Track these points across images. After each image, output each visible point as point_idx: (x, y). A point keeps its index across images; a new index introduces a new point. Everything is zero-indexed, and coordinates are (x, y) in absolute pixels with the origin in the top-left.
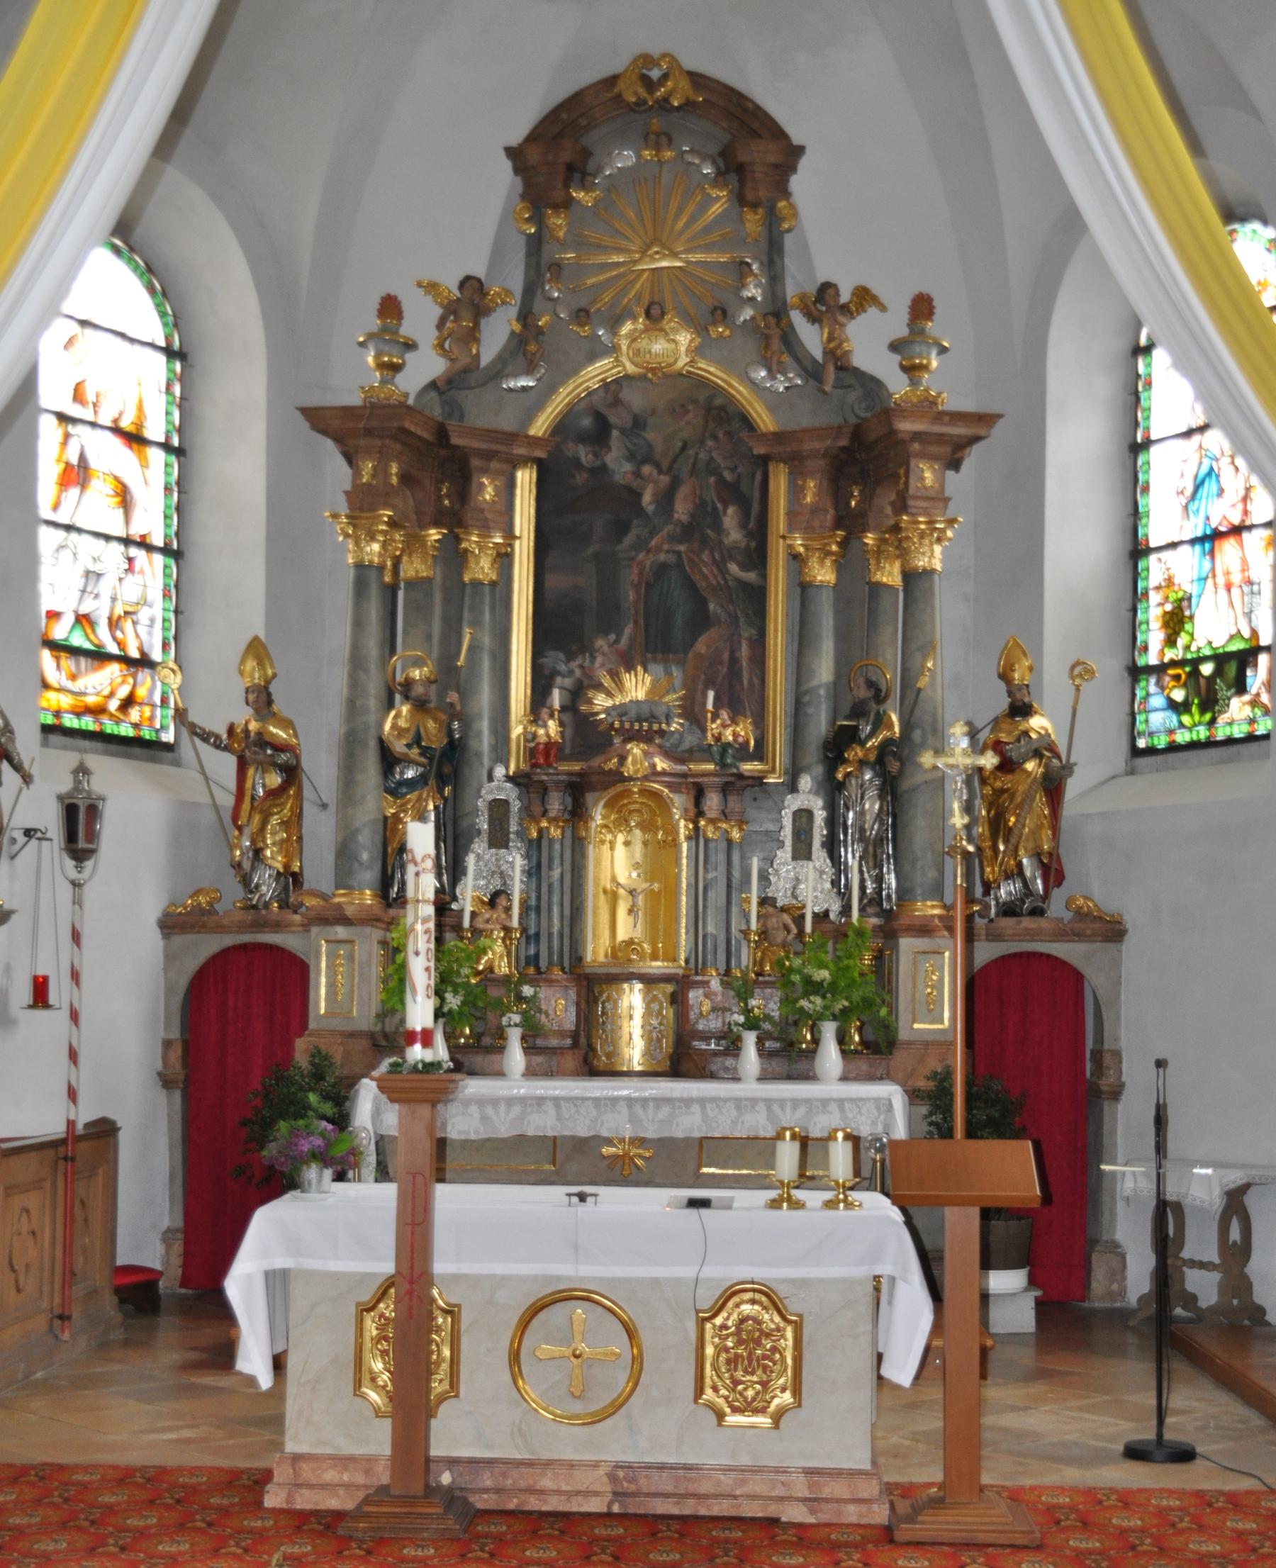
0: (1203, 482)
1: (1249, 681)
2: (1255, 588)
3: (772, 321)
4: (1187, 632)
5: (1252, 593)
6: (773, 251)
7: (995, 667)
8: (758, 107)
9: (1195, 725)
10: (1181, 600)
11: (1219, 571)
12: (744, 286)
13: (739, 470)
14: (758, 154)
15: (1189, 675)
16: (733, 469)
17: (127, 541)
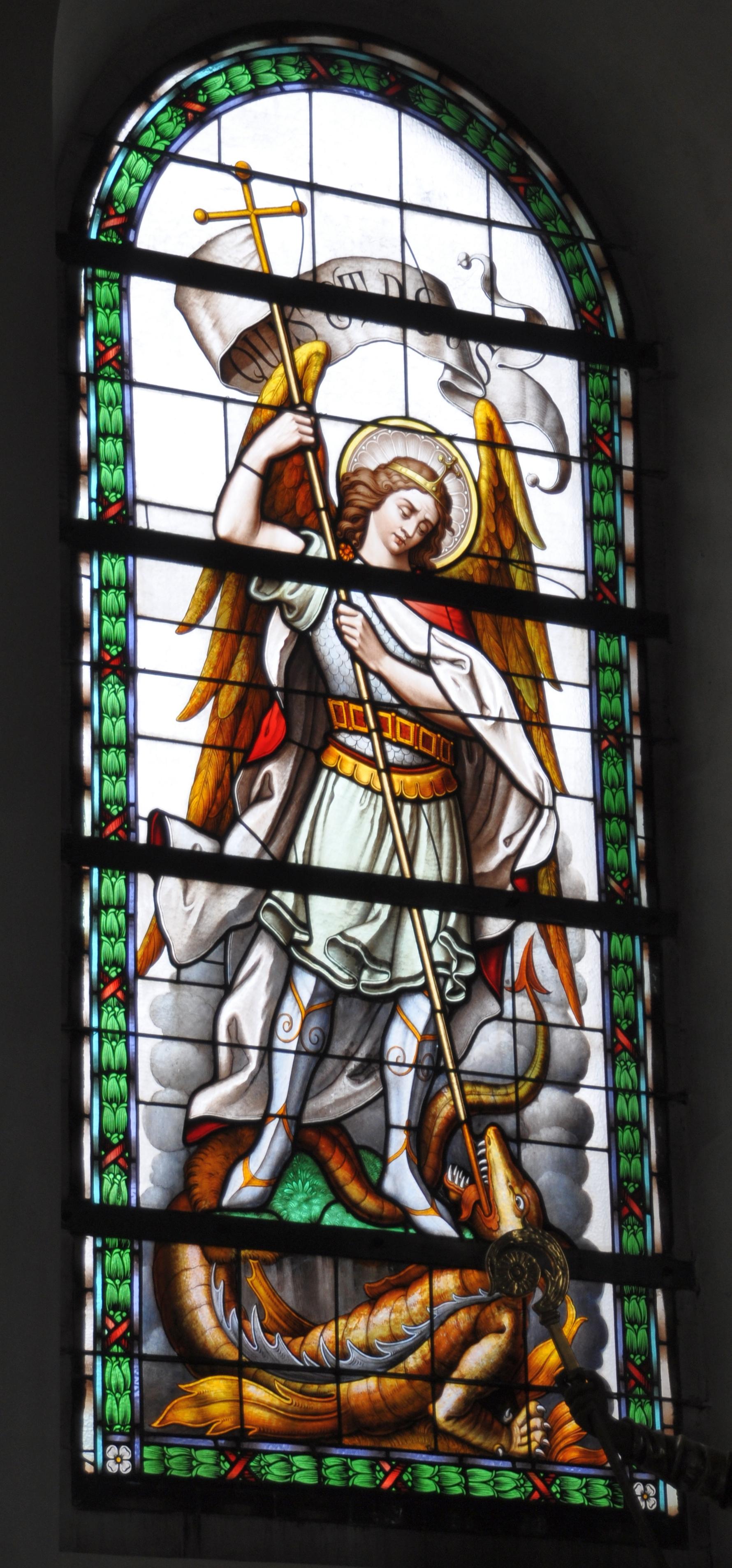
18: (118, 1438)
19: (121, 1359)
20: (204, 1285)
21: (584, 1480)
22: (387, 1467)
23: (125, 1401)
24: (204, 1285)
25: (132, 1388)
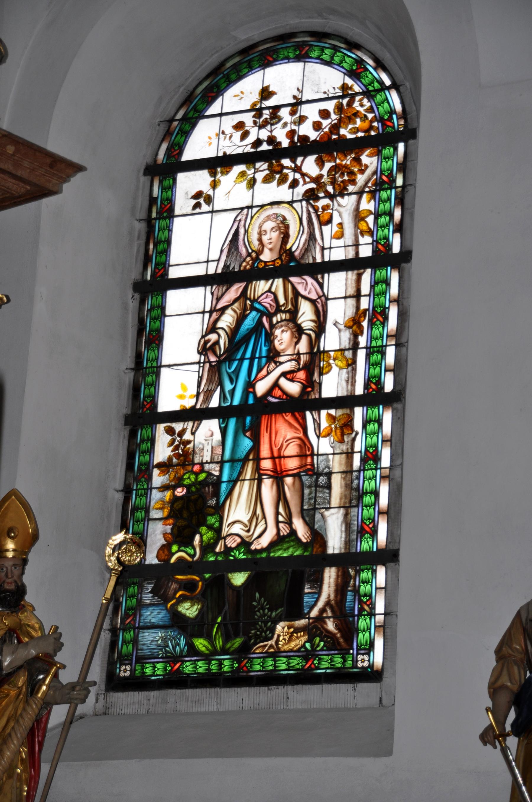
0: (246, 339)
1: (307, 600)
2: (322, 480)
4: (210, 527)
5: (317, 485)
9: (214, 652)
10: (204, 483)
11: (265, 452)
15: (208, 584)
17: (345, 246)
18: (363, 652)
19: (366, 617)
20: (405, 298)
21: (383, 160)
22: (375, 320)
23: (200, 663)
24: (405, 298)
25: (370, 629)
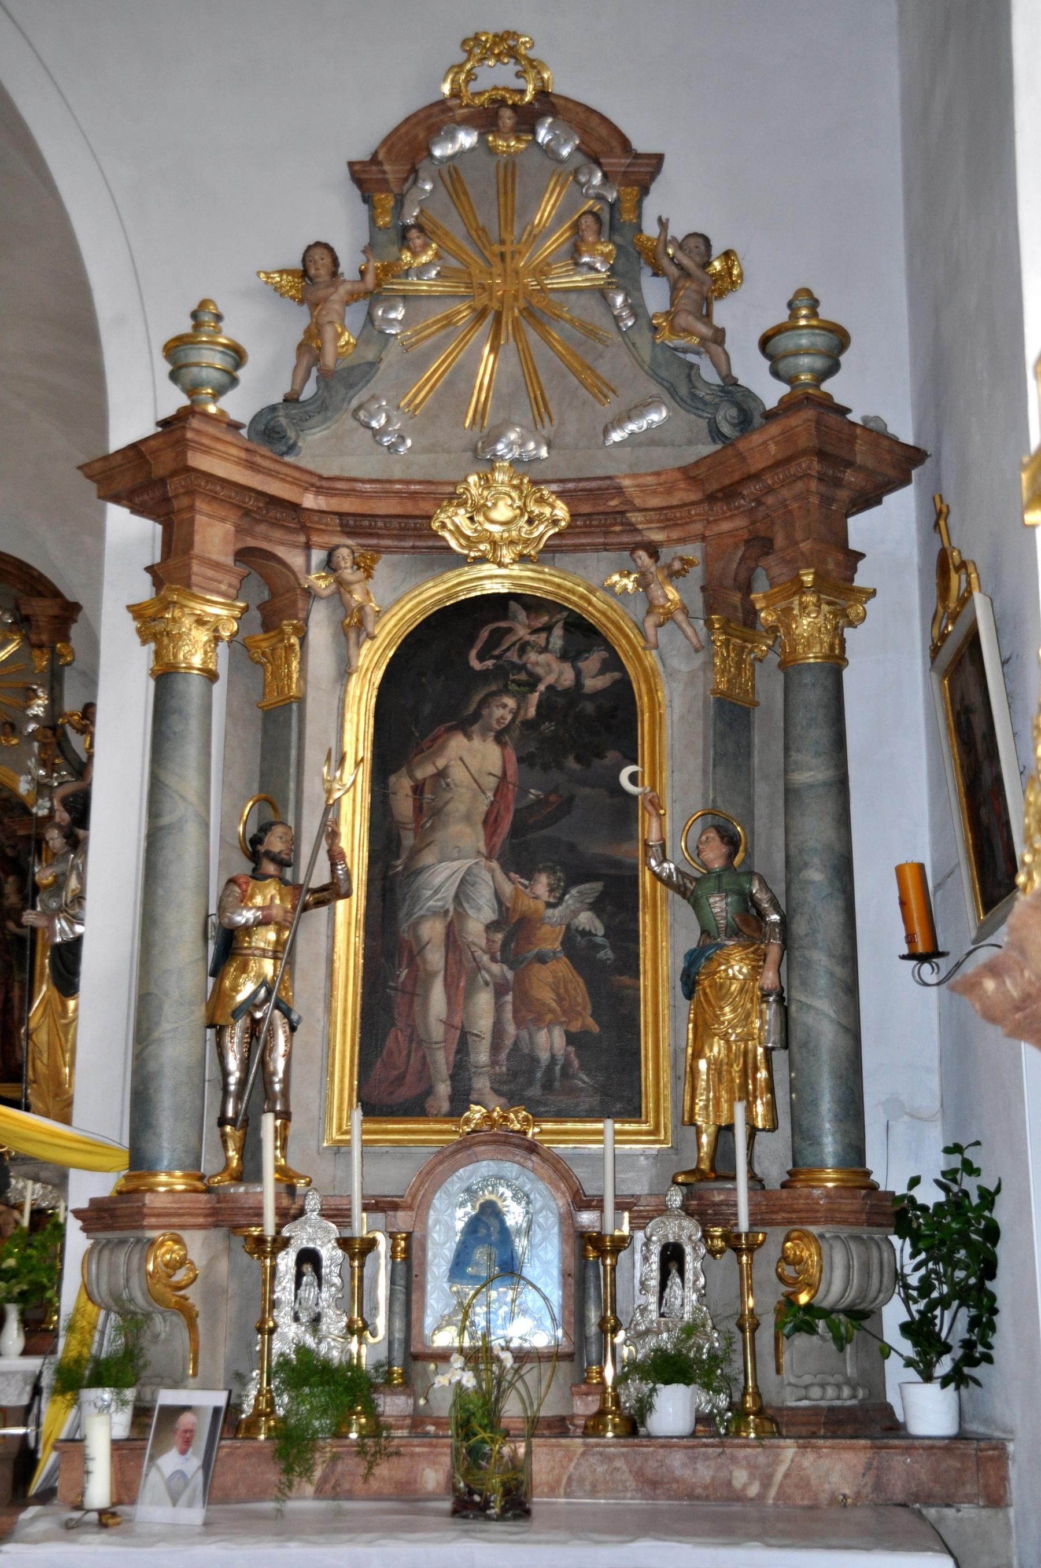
3: (49, 733)
6: (54, 683)
7: (744, 264)
8: (41, 575)
12: (29, 707)
13: (19, 847)
14: (41, 609)
16: (14, 847)
